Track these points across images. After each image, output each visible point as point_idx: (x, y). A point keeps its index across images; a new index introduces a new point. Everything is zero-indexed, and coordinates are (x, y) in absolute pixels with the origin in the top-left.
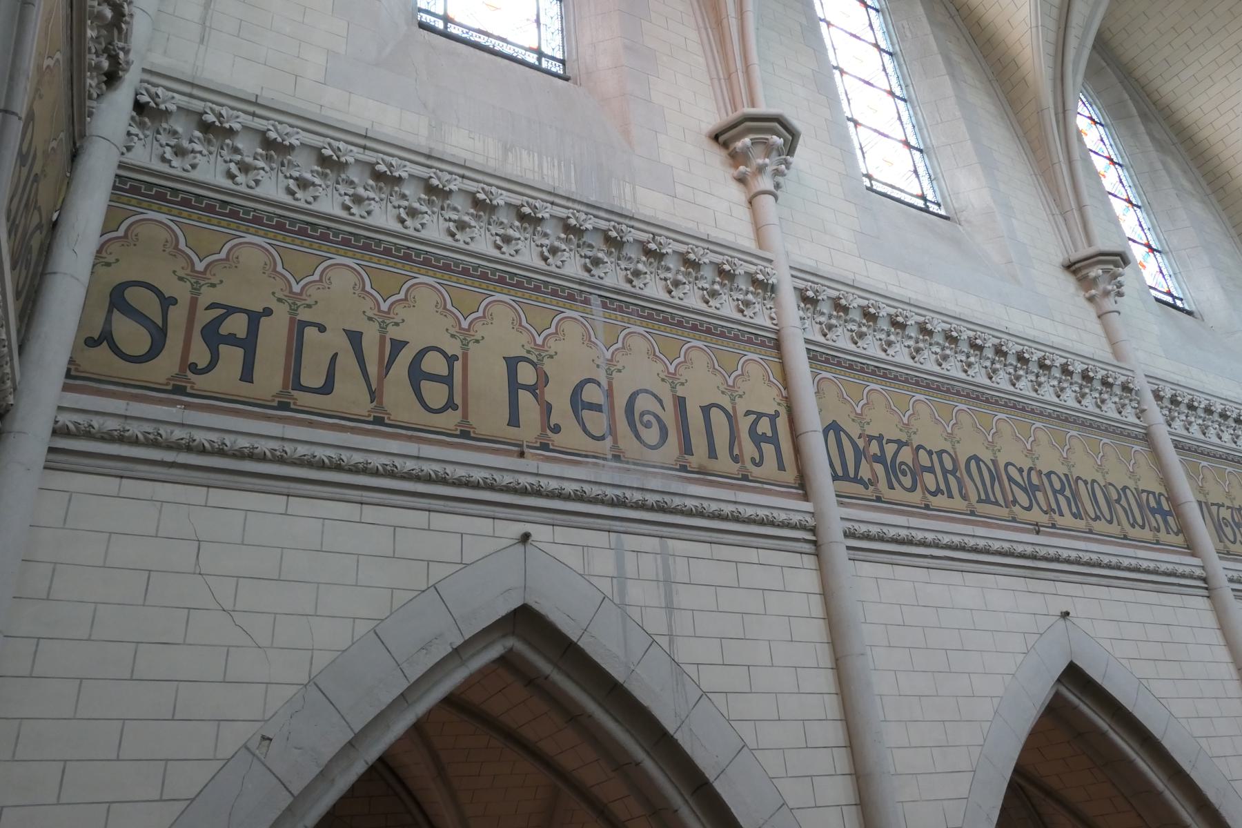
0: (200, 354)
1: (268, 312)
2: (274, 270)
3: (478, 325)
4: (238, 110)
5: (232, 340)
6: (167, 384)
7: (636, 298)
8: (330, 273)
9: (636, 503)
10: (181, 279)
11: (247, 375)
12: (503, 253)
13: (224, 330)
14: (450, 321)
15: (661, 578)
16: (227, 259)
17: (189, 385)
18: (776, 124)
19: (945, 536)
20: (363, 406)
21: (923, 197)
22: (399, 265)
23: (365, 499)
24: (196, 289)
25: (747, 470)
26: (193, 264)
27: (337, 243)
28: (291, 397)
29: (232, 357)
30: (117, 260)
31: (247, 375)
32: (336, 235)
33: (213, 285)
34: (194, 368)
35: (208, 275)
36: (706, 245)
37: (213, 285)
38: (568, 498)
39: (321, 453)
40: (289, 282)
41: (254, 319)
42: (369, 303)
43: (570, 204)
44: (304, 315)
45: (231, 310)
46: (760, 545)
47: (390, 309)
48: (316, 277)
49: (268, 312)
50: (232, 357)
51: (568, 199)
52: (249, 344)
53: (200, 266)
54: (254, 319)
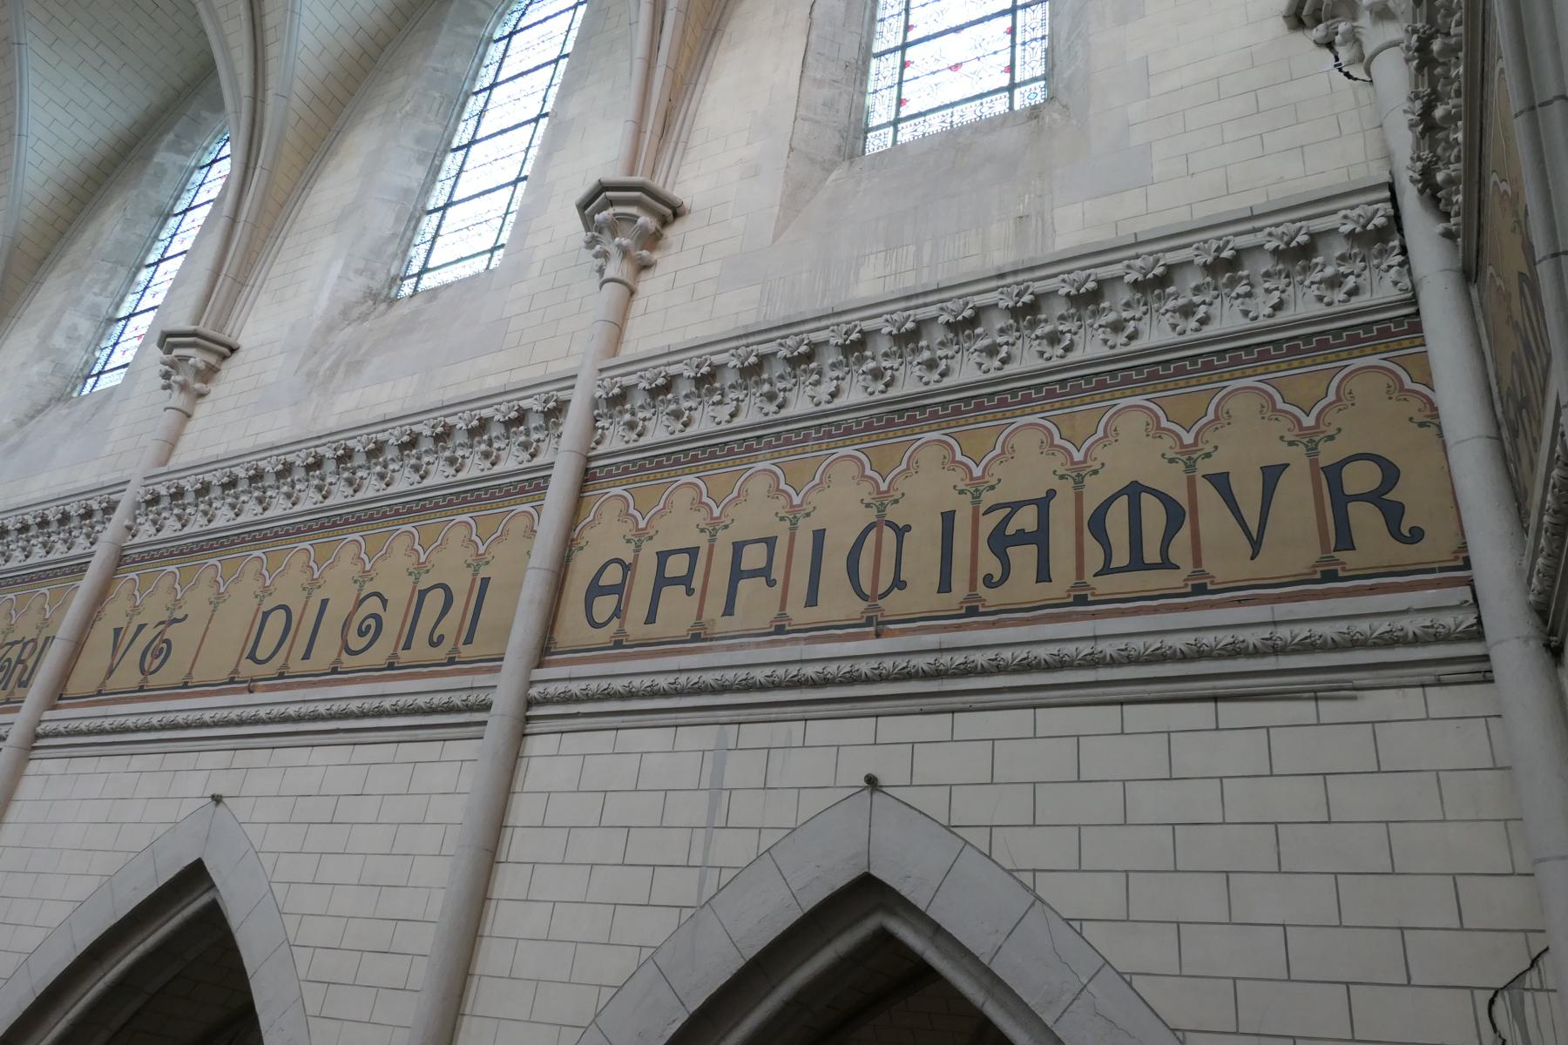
0: (989, 564)
1: (1051, 494)
2: (1159, 427)
3: (1208, 435)
4: (1300, 220)
5: (1022, 538)
6: (1456, 558)
7: (827, 416)
8: (1014, 440)
9: (1380, 636)
10: (1291, 443)
11: (1043, 575)
12: (1330, 304)
13: (1011, 530)
14: (1284, 424)
15: (705, 784)
16: (1217, 418)
17: (1338, 567)
18: (609, 194)
19: (1376, 622)
20: (855, 608)
21: (425, 269)
22: (1097, 398)
23: (807, 715)
24: (976, 497)
25: (1086, 586)
26: (1181, 440)
27: (1044, 398)
28: (1337, 562)
29: (1024, 558)
30: (1339, 430)
31: (1043, 575)
32: (1014, 395)
33: (1331, 438)
34: (988, 581)
35: (1323, 428)
36: (744, 341)
37: (1331, 438)
38: (867, 680)
39: (1043, 653)
40: (1178, 435)
41: (1043, 505)
42: (1168, 441)
43: (1258, 224)
44: (1329, 454)
45: (1015, 506)
46: (741, 719)
47: (1318, 419)
48: (783, 486)
49: (1051, 494)
50: (1024, 558)
51: (819, 318)
52: (1040, 538)
53: (1188, 439)
54: (1043, 505)
